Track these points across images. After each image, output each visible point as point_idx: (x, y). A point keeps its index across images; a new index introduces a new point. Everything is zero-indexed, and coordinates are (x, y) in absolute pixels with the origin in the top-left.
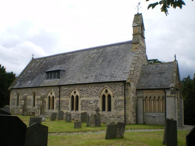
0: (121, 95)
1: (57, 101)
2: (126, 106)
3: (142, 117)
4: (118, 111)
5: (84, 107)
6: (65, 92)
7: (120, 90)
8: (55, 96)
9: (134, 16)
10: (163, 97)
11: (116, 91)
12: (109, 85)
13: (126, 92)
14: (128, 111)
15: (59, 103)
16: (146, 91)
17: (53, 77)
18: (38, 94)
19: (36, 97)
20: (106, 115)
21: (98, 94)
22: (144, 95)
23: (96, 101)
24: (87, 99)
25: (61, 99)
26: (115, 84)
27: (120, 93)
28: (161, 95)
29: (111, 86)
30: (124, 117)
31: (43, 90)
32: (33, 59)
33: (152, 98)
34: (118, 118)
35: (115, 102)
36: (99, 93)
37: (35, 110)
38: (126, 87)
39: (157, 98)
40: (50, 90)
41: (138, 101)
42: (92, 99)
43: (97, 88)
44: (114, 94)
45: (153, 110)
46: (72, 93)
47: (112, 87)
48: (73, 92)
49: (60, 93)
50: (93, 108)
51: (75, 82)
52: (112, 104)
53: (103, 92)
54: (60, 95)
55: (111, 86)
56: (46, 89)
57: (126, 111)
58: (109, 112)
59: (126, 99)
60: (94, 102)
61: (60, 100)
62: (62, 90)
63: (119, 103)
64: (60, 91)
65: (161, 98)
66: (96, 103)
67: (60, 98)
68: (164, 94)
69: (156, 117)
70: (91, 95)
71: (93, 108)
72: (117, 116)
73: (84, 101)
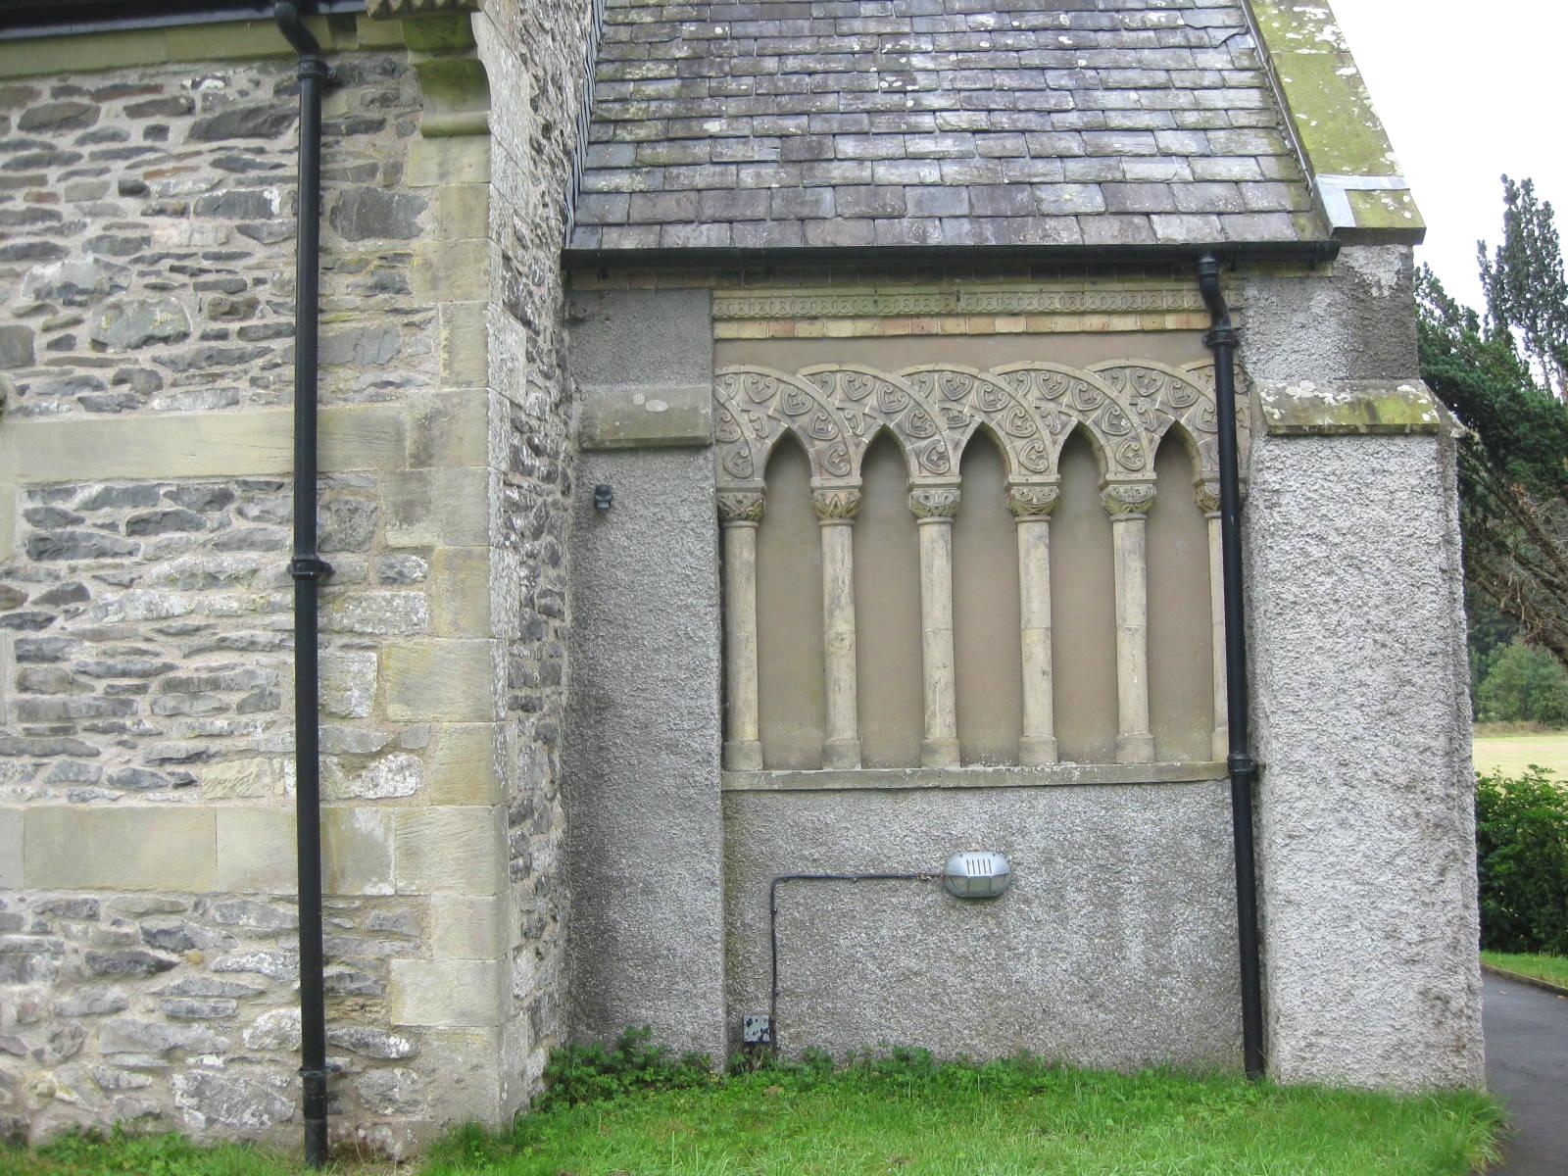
2: (329, 652)
3: (710, 902)
4: (104, 799)
7: (170, 233)
10: (1173, 444)
11: (50, 272)
13: (339, 289)
14: (390, 777)
16: (782, 300)
22: (736, 395)
27: (162, 319)
30: (280, 959)
35: (42, 549)
38: (349, 153)
41: (616, 535)
45: (941, 726)
57: (334, 780)
59: (341, 455)
68: (1196, 374)
69: (1032, 882)
72: (77, 940)
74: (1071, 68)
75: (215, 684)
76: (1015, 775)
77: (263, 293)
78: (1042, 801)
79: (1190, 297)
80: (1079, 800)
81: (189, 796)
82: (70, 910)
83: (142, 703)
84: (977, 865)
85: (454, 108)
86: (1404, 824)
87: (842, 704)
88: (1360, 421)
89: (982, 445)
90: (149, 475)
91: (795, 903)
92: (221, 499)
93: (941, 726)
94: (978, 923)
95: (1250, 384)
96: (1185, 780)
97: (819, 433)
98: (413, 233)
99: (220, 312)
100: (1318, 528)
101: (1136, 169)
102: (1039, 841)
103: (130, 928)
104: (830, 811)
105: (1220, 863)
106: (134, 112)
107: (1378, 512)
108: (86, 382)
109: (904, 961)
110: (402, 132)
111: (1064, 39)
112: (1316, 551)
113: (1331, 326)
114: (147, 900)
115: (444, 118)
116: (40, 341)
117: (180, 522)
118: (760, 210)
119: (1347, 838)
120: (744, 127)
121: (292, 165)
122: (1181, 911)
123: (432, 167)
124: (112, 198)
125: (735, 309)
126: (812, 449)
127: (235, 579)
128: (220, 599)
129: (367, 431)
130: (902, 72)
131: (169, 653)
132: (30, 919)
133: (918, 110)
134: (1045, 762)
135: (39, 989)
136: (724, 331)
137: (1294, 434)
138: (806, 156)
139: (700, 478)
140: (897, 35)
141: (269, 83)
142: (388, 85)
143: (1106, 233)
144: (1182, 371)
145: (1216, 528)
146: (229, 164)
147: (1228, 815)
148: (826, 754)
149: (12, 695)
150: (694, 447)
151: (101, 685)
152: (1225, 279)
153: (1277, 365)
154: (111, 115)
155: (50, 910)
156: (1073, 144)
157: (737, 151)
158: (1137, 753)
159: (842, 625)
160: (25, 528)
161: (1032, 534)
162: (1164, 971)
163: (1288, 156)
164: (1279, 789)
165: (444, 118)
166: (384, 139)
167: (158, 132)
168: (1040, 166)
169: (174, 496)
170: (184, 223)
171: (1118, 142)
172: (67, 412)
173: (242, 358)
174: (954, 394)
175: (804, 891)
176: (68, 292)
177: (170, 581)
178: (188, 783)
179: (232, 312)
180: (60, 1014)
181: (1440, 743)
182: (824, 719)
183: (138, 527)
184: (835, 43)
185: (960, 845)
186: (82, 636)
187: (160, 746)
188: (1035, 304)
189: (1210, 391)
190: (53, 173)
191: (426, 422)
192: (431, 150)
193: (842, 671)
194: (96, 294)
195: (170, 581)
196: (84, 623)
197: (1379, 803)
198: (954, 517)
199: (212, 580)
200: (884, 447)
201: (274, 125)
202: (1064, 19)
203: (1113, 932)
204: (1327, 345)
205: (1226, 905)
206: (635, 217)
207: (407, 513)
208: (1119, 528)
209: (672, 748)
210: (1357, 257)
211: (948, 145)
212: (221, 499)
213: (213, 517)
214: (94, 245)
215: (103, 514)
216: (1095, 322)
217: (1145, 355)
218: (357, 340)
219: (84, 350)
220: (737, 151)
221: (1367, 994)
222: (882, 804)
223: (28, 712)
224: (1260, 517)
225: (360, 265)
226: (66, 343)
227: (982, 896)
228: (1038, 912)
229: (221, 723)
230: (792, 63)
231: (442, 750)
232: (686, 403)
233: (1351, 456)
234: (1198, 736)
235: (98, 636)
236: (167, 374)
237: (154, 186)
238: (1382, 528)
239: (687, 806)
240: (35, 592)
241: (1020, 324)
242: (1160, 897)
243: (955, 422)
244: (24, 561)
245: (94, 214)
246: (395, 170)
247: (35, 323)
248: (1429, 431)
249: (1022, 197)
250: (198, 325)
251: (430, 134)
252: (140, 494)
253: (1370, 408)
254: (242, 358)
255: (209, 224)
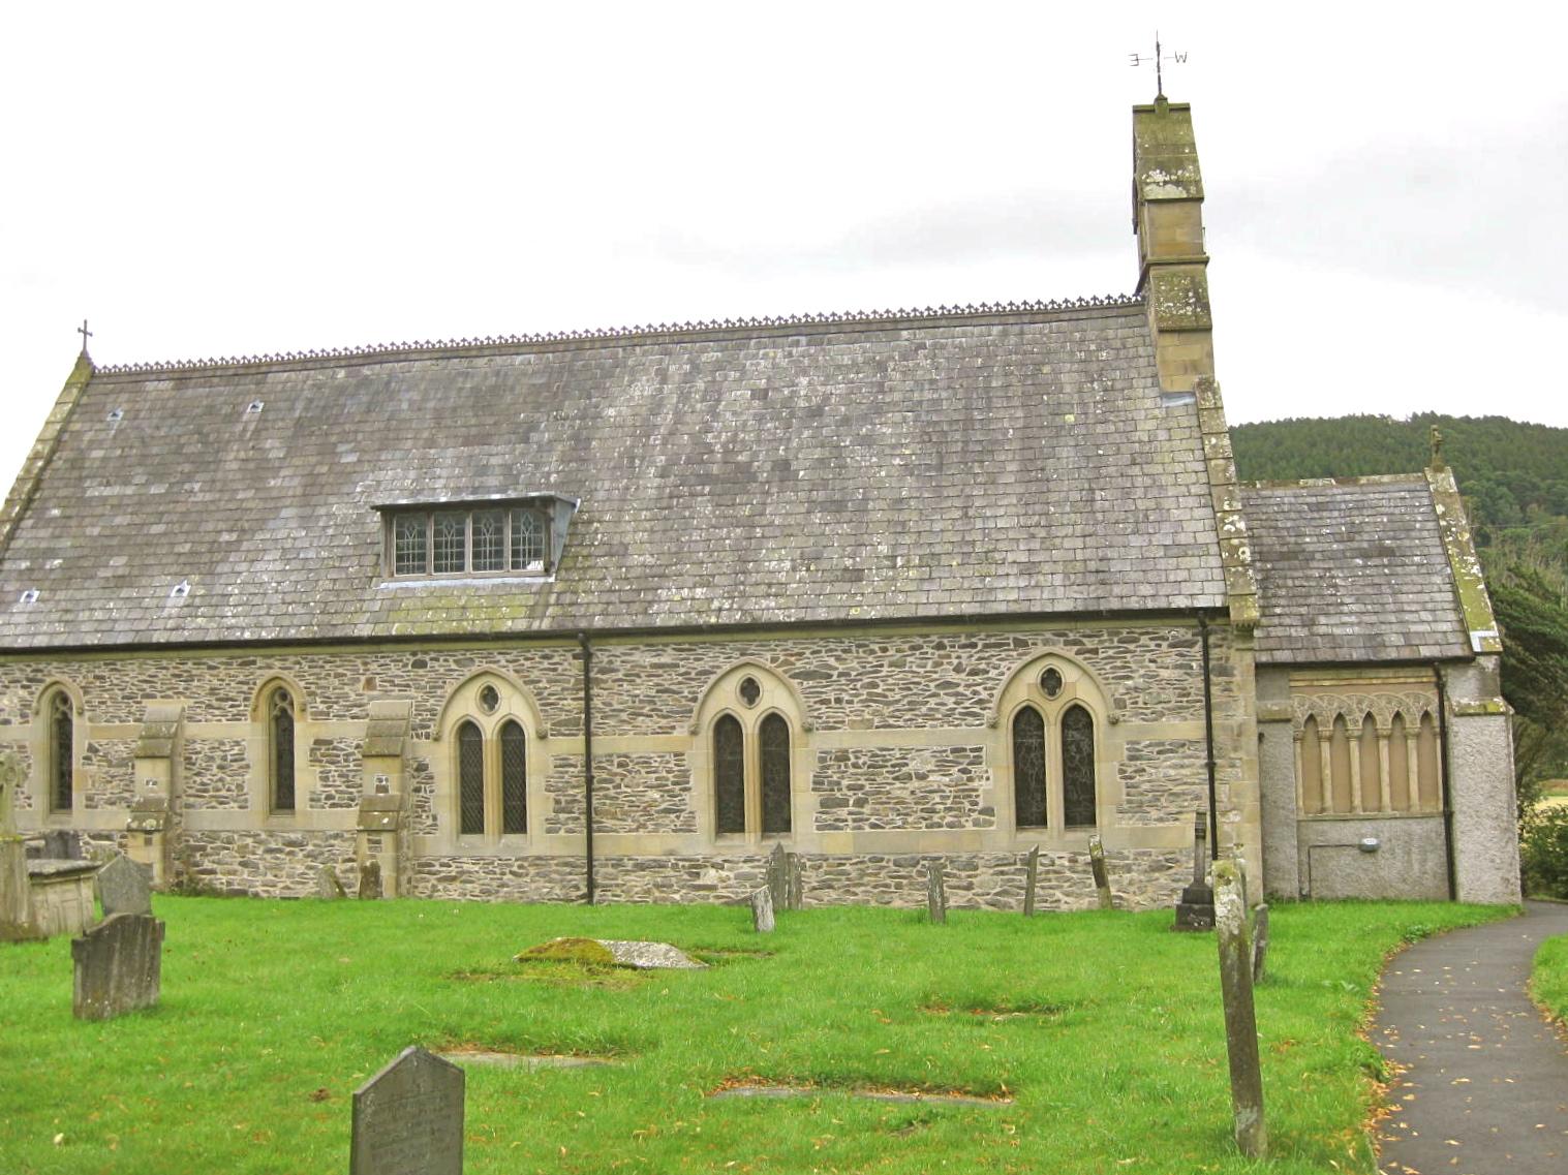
0: (1178, 710)
1: (563, 763)
2: (1216, 784)
4: (1153, 825)
5: (844, 803)
6: (644, 688)
7: (1164, 674)
8: (538, 722)
9: (1127, 119)
10: (1426, 715)
11: (1130, 683)
12: (1071, 636)
13: (1214, 690)
14: (1233, 817)
15: (589, 780)
17: (469, 560)
18: (326, 700)
19: (298, 727)
20: (1051, 855)
21: (980, 702)
23: (965, 758)
24: (873, 740)
25: (601, 745)
26: (1125, 628)
27: (1163, 697)
28: (1410, 701)
29: (1089, 644)
31: (396, 666)
32: (88, 380)
33: (1355, 726)
34: (1153, 869)
35: (1132, 758)
36: (984, 695)
37: (291, 844)
38: (1214, 653)
39: (1384, 722)
40: (468, 673)
42: (920, 742)
43: (968, 658)
44: (1120, 704)
46: (727, 698)
47: (1095, 651)
48: (733, 683)
49: (588, 699)
50: (934, 811)
51: (751, 604)
52: (1106, 775)
53: (1026, 690)
54: (588, 710)
55: (1089, 644)
56: (421, 664)
58: (1079, 835)
60: (943, 766)
61: (596, 750)
62: (603, 671)
63: (1164, 769)
64: (588, 683)
65: (1413, 723)
66: (963, 771)
67: (588, 735)
69: (1385, 847)
70: (914, 710)
71: (934, 811)
72: (1145, 862)
73: (842, 757)
74: (1389, 584)
75: (1184, 794)
76: (1380, 815)
77: (1193, 691)
78: (1388, 823)
79: (1430, 672)
80: (1398, 822)
81: (1177, 823)
82: (1144, 854)
83: (1163, 799)
84: (1370, 841)
85: (1244, 642)
86: (1495, 829)
87: (1328, 795)
88: (1482, 711)
89: (1369, 717)
90: (1162, 738)
91: (1315, 854)
92: (1183, 745)
93: (1357, 801)
94: (1369, 859)
95: (1449, 699)
96: (1429, 816)
97: (1320, 714)
98: (1232, 675)
99: (1180, 695)
100: (1469, 742)
101: (1414, 628)
102: (1387, 835)
103: (1161, 858)
104: (1326, 826)
105: (1441, 841)
106: (1151, 639)
107: (1487, 738)
108: (1142, 714)
109: (1348, 871)
110: (1229, 648)
111: (1386, 571)
112: (1469, 749)
113: (1473, 681)
114: (1166, 851)
115: (1242, 646)
116: (1128, 702)
117: (1172, 751)
118: (1300, 646)
119: (1479, 833)
120: (1287, 610)
121: (1199, 656)
122: (1430, 856)
123: (1238, 658)
124: (1147, 663)
125: (1297, 677)
126: (1319, 719)
127: (1188, 766)
128: (1184, 771)
129: (1224, 728)
130: (1335, 586)
131: (1170, 786)
132: (1132, 857)
133: (1342, 604)
134: (1389, 812)
135: (1134, 875)
136: (1293, 684)
137: (1462, 715)
138: (1309, 623)
139: (1289, 729)
140: (1330, 569)
141: (1190, 633)
142: (1224, 635)
143: (1406, 654)
144: (1429, 694)
145: (1439, 741)
146: (1181, 655)
147: (1443, 827)
148: (1323, 810)
149: (1125, 797)
150: (1288, 721)
151: (1150, 795)
152: (1441, 667)
153: (1457, 692)
154: (1144, 640)
155: (1139, 854)
156: (1393, 618)
157: (1287, 621)
158: (1416, 809)
159: (1328, 771)
160: (1126, 753)
161: (1383, 743)
162: (1425, 873)
163: (1461, 621)
164: (1460, 822)
165: (1242, 646)
166: (1224, 649)
167: (1159, 646)
168: (1383, 627)
169: (1170, 744)
170: (1169, 671)
171: (1407, 617)
172: (1136, 722)
173: (1188, 708)
174: (1360, 702)
175: (1318, 850)
176: (1136, 689)
177: (1170, 767)
178: (1177, 819)
179: (1184, 696)
180: (1141, 881)
181: (1506, 806)
182: (1322, 798)
183: (1159, 753)
184: (1309, 572)
185: (1364, 836)
186: (1144, 781)
187: (1168, 810)
188: (1384, 675)
189: (1437, 700)
190: (1129, 655)
191: (1240, 726)
192: (1238, 654)
193: (1328, 785)
194: (1144, 690)
195: (1170, 767)
196: (1145, 778)
197: (1488, 823)
198: (1360, 739)
199: (1182, 767)
200: (1340, 717)
201: (1191, 644)
202: (1386, 561)
203: (1409, 861)
204: (1472, 686)
205: (1443, 853)
206: (1263, 647)
207: (1235, 749)
208: (1409, 741)
209: (1283, 808)
210: (1482, 660)
211: (1353, 619)
212: (1183, 745)
213: (1181, 750)
214: (1143, 676)
215: (1150, 749)
216: (1402, 680)
217: (1417, 690)
218: (1220, 704)
219: (1141, 705)
220: (1287, 621)
221: (1485, 878)
222: (1341, 824)
223: (1129, 802)
224: (1452, 739)
225: (1219, 684)
226: (1136, 703)
227: (1370, 851)
228: (1387, 856)
229: (1186, 804)
230: (1297, 583)
231: (1246, 810)
232: (1283, 707)
233: (1479, 722)
234: (1433, 803)
235: (1149, 781)
236: (1167, 712)
237: (1159, 660)
238: (1488, 742)
239: (1288, 825)
240: (1130, 770)
241: (1379, 681)
242: (1423, 851)
243: (1361, 711)
244: (1127, 762)
245: (1142, 667)
246: (1227, 659)
247: (1126, 697)
248: (1502, 714)
249: (1379, 639)
250: (1174, 699)
251: (1238, 650)
252: (1163, 744)
253: (1485, 707)
254: (1188, 708)
255: (1176, 671)
